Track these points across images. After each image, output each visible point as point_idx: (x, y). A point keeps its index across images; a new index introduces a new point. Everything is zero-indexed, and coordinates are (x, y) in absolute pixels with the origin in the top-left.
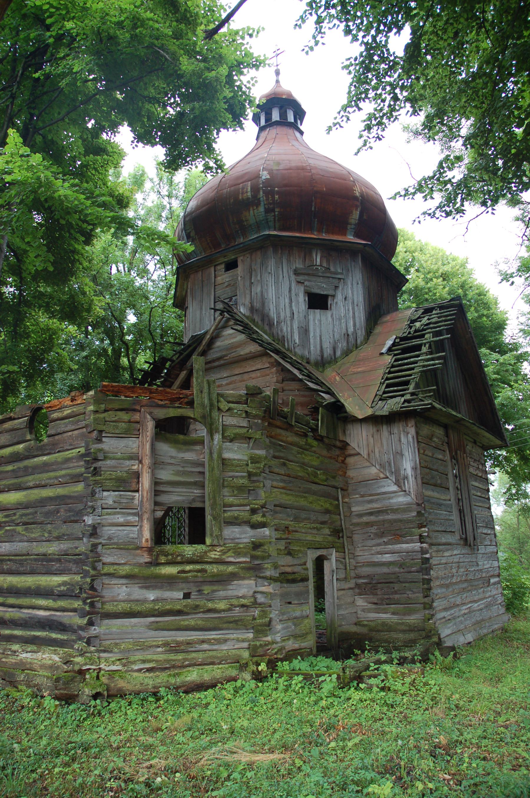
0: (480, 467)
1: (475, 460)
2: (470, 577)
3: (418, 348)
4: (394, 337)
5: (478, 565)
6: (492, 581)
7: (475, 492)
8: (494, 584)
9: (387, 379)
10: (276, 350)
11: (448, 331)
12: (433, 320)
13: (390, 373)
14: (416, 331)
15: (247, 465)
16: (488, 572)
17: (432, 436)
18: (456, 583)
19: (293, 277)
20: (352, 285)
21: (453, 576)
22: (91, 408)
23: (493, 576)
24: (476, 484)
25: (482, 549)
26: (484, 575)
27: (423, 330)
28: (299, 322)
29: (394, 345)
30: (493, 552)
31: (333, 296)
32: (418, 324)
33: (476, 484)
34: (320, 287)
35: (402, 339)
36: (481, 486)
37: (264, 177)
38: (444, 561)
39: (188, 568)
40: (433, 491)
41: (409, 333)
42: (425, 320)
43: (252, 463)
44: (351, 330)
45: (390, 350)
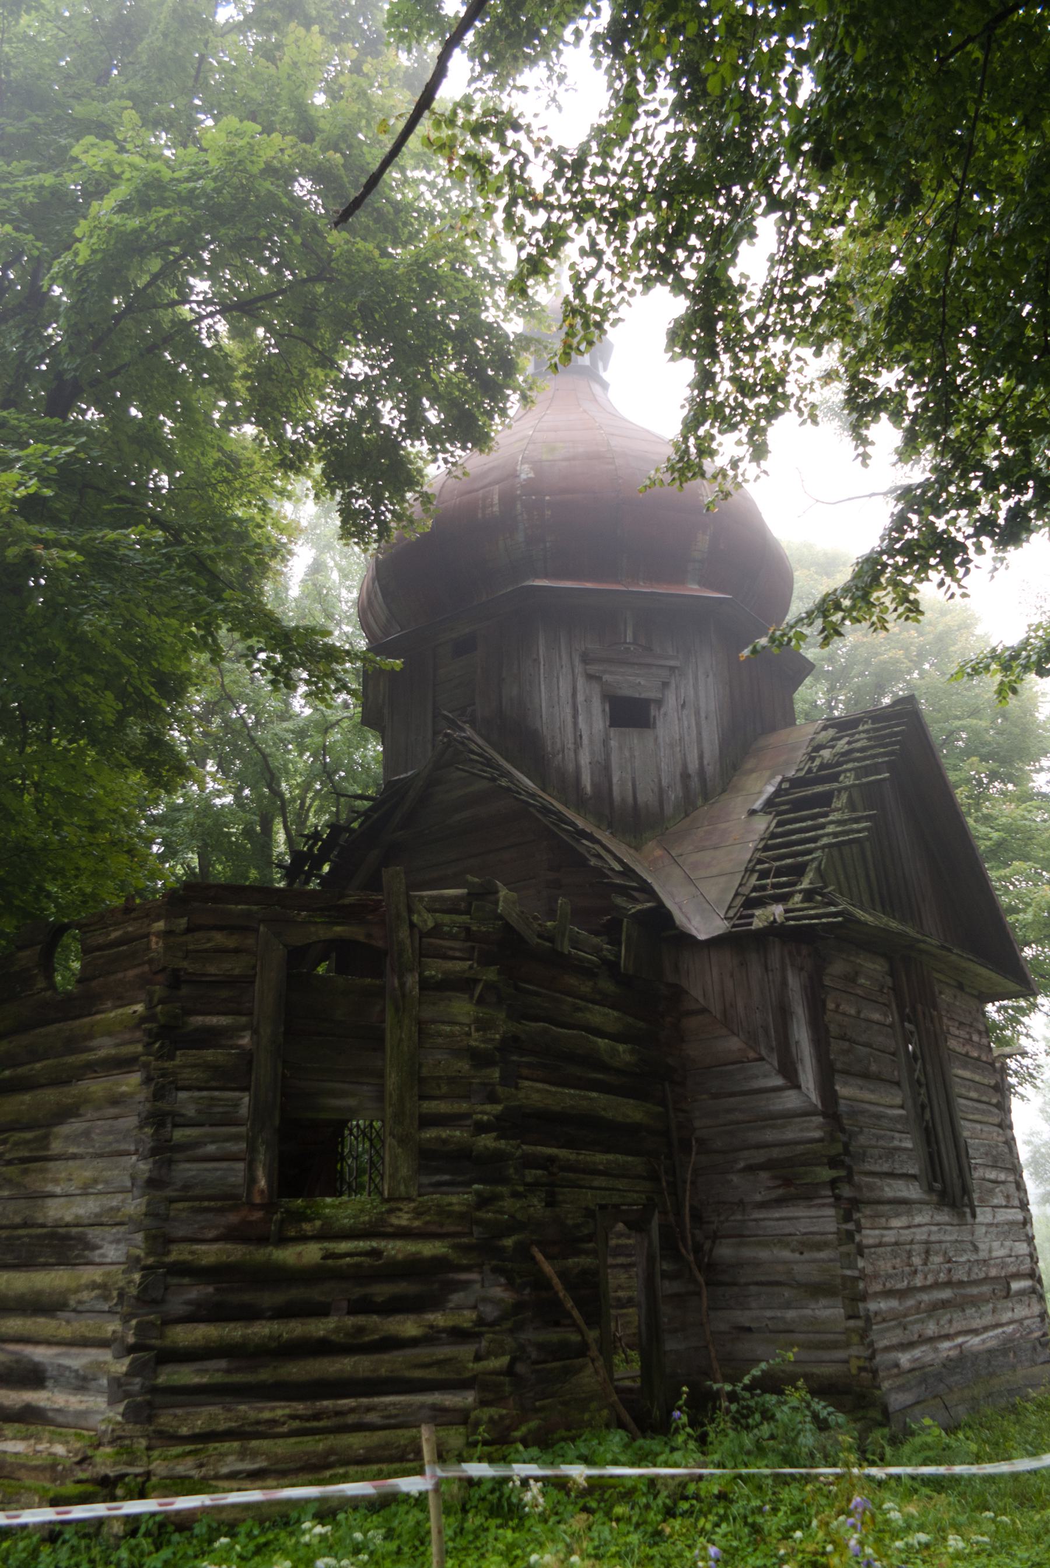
0: (975, 1038)
1: (961, 1024)
2: (960, 1275)
3: (825, 800)
4: (779, 778)
5: (976, 1249)
6: (1015, 1286)
7: (963, 1091)
8: (1022, 1293)
9: (760, 862)
10: (544, 807)
11: (891, 766)
12: (858, 745)
13: (766, 848)
14: (822, 767)
15: (469, 1034)
16: (1003, 1265)
17: (857, 973)
18: (924, 1289)
19: (579, 668)
20: (696, 678)
21: (915, 1272)
22: (160, 925)
23: (1017, 1276)
24: (967, 1074)
25: (984, 1215)
26: (993, 1272)
27: (839, 764)
28: (592, 753)
29: (778, 793)
30: (1012, 1223)
31: (659, 703)
32: (826, 753)
33: (967, 1074)
34: (634, 683)
35: (796, 783)
36: (977, 1078)
37: (523, 476)
38: (890, 1237)
39: (344, 1246)
40: (872, 1091)
41: (810, 770)
42: (842, 745)
43: (477, 1030)
44: (693, 767)
45: (770, 803)
